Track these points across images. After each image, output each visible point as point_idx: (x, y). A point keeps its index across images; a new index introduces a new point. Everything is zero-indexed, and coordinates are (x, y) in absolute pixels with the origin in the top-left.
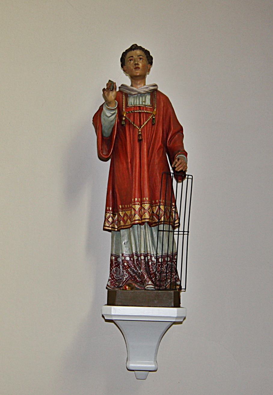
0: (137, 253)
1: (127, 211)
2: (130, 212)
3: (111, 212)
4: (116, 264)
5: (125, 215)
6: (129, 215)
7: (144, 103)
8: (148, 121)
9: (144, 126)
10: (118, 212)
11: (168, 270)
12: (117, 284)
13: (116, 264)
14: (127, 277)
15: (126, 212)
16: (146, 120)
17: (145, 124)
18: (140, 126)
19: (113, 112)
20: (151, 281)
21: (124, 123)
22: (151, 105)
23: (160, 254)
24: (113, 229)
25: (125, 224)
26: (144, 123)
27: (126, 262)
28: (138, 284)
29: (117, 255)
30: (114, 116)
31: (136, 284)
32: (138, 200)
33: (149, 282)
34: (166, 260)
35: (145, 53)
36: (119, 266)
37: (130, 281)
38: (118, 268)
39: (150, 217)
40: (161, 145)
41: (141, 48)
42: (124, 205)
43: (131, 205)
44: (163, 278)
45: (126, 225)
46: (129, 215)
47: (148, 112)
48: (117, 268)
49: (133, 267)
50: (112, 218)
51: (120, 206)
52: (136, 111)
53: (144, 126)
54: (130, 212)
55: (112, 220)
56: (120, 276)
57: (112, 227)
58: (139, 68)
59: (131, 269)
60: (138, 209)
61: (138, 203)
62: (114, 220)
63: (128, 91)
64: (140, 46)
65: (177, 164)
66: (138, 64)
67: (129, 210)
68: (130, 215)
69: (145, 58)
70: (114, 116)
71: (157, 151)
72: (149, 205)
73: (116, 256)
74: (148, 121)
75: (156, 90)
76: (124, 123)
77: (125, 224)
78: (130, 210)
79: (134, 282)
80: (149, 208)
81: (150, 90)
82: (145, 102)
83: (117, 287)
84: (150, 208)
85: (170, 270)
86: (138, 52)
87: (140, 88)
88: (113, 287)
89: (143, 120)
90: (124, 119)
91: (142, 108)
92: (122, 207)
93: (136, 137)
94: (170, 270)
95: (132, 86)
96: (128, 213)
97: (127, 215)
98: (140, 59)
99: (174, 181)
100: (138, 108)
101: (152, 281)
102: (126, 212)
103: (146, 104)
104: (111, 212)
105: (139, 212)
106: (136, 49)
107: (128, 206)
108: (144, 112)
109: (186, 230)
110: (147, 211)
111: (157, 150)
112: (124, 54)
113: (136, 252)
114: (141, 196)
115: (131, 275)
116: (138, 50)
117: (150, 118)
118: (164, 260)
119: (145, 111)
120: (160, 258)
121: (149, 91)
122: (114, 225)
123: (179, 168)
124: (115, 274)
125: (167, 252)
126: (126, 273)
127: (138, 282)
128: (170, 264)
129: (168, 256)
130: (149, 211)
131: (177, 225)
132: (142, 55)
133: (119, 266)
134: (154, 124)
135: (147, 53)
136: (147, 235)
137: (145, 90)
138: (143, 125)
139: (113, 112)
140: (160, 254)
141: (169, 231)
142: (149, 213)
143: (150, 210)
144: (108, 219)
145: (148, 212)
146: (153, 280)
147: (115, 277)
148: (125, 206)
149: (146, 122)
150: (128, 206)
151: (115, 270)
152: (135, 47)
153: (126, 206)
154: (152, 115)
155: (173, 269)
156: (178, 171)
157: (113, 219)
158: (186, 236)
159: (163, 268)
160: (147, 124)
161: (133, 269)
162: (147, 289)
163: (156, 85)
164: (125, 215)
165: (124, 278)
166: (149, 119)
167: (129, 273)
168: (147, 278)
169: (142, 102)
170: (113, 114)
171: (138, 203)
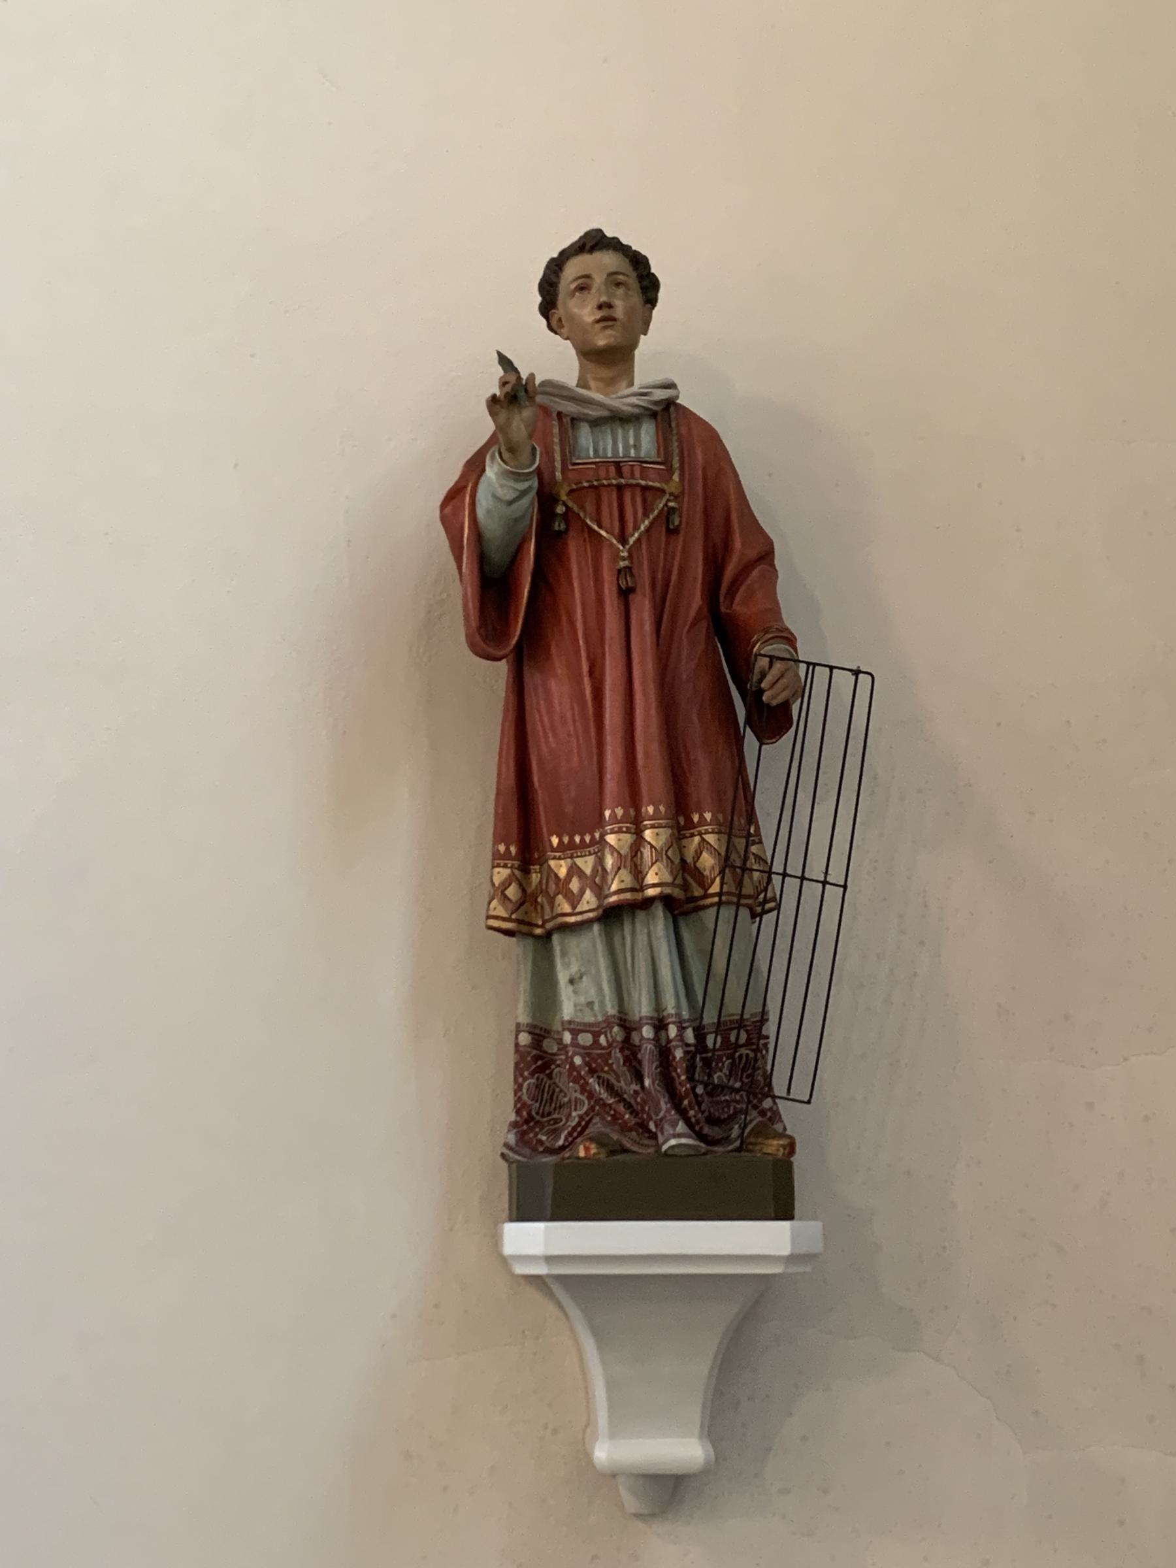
0: (624, 1017)
1: (581, 856)
2: (591, 860)
3: (516, 863)
4: (539, 1063)
5: (574, 870)
6: (588, 871)
7: (632, 453)
8: (651, 517)
9: (639, 540)
10: (543, 861)
11: (741, 1080)
12: (544, 1138)
13: (539, 1063)
14: (581, 1112)
15: (579, 862)
16: (646, 515)
17: (642, 528)
18: (623, 540)
19: (523, 486)
20: (683, 1119)
21: (563, 527)
22: (659, 460)
23: (710, 1018)
24: (524, 928)
25: (574, 908)
26: (639, 528)
27: (582, 1051)
28: (629, 1134)
29: (541, 1029)
30: (525, 501)
31: (626, 1136)
32: (613, 814)
33: (677, 1125)
34: (733, 1039)
35: (631, 261)
36: (548, 1072)
37: (599, 1125)
38: (545, 1079)
39: (675, 879)
40: (700, 608)
41: (615, 245)
42: (568, 834)
43: (597, 835)
44: (724, 1112)
45: (579, 909)
46: (588, 871)
47: (651, 483)
48: (542, 1076)
49: (605, 1072)
50: (520, 885)
51: (651, 809)
52: (605, 482)
53: (640, 535)
54: (591, 860)
55: (520, 895)
56: (552, 1109)
57: (519, 922)
58: (614, 320)
59: (599, 1077)
60: (628, 850)
61: (628, 825)
62: (529, 891)
63: (570, 408)
64: (614, 238)
65: (769, 678)
66: (610, 306)
67: (590, 854)
68: (595, 871)
69: (632, 279)
70: (525, 501)
71: (689, 631)
72: (669, 831)
73: (538, 1031)
74: (654, 519)
75: (670, 405)
76: (563, 527)
77: (574, 908)
78: (595, 853)
79: (617, 1128)
80: (672, 845)
81: (656, 403)
82: (637, 447)
83: (542, 1152)
84: (674, 845)
85: (746, 1081)
86: (608, 260)
87: (623, 399)
88: (527, 1151)
89: (635, 514)
90: (560, 509)
91: (626, 470)
92: (561, 841)
93: (608, 577)
94: (747, 1077)
95: (583, 383)
96: (587, 864)
97: (581, 873)
98: (618, 284)
99: (750, 741)
100: (612, 469)
101: (688, 1122)
102: (579, 862)
103: (642, 454)
104: (516, 863)
105: (632, 858)
106: (601, 249)
107: (587, 838)
108: (638, 485)
109: (836, 876)
110: (664, 857)
111: (687, 627)
112: (555, 267)
113: (620, 1012)
114: (633, 797)
115: (599, 1101)
116: (607, 250)
117: (661, 505)
118: (726, 1040)
119: (643, 483)
120: (712, 1033)
121: (651, 407)
122: (526, 913)
123: (778, 695)
124: (537, 1101)
125: (740, 1012)
126: (582, 1093)
127: (630, 1130)
128: (747, 1055)
129: (740, 1024)
130: (669, 853)
131: (772, 905)
132: (621, 271)
133: (548, 1072)
134: (676, 531)
135: (639, 262)
136: (824, 810)
137: (634, 400)
138: (636, 535)
139: (523, 486)
140: (710, 1018)
141: (785, 875)
142: (672, 862)
143: (674, 853)
144: (506, 889)
145: (668, 857)
146: (690, 1118)
147: (533, 1113)
148: (572, 840)
149: (647, 522)
150: (587, 838)
151: (537, 1087)
152: (594, 242)
153: (577, 839)
154: (667, 496)
155: (757, 1073)
156: (774, 703)
157: (524, 890)
158: (833, 894)
159: (721, 1071)
160: (648, 530)
161: (608, 1080)
162: (670, 1152)
163: (671, 386)
164: (574, 870)
165: (574, 1114)
166: (656, 512)
167: (591, 1095)
168: (668, 1111)
169: (626, 447)
170: (523, 493)
171: (628, 825)
